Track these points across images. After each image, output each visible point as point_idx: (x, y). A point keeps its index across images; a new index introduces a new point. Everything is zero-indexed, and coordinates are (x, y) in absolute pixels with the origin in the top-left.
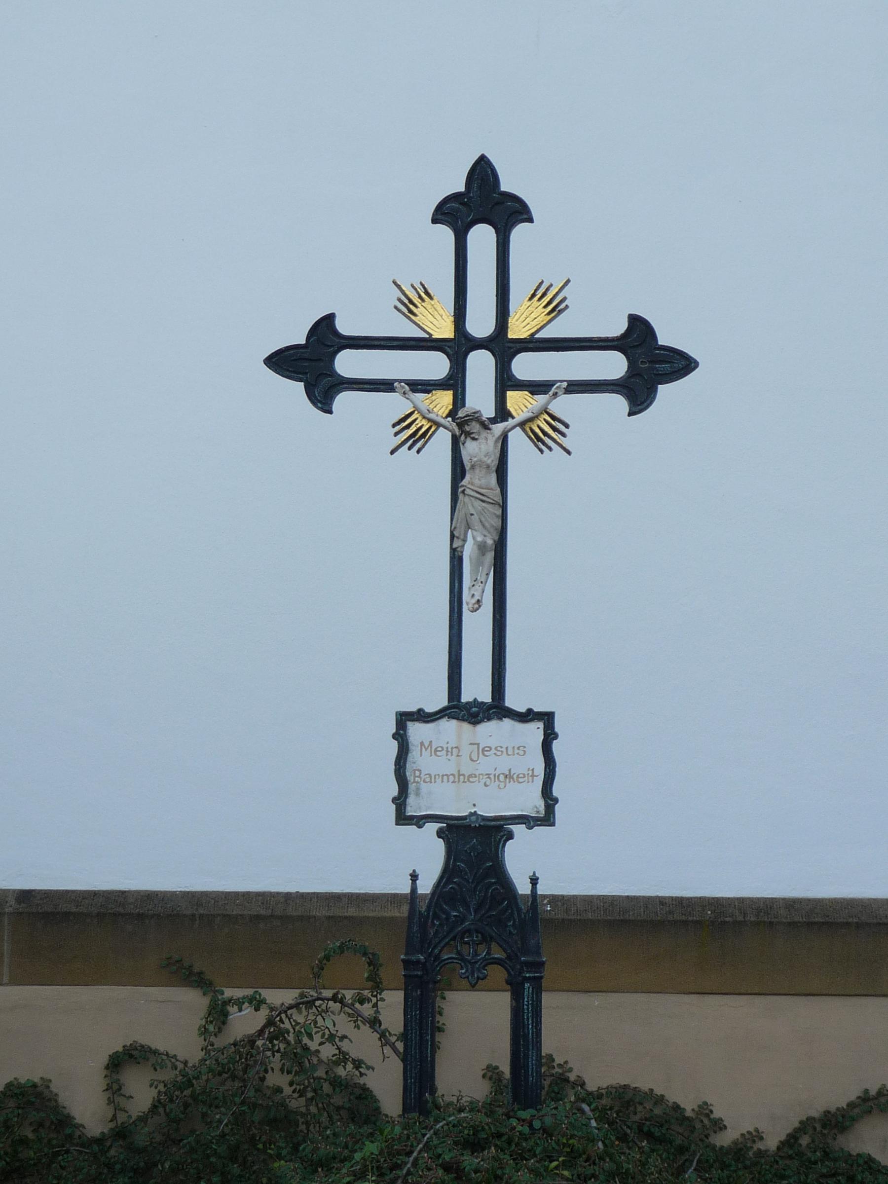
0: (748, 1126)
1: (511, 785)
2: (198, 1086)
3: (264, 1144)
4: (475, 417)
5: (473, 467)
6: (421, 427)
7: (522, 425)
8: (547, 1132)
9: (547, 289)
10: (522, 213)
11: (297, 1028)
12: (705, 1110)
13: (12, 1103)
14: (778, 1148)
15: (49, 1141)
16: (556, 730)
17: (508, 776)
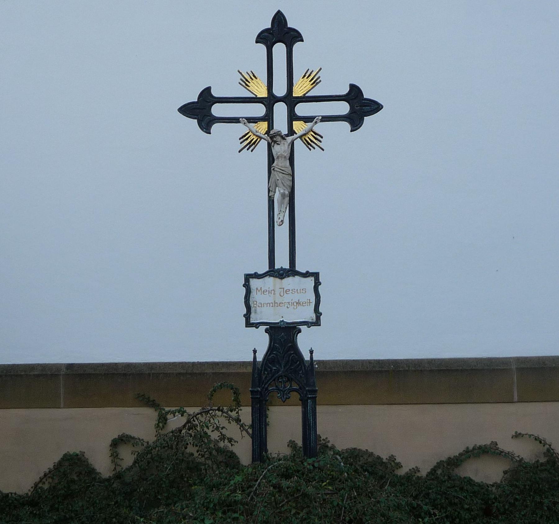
0: (412, 466)
1: (300, 308)
2: (154, 452)
3: (187, 478)
4: (279, 134)
5: (278, 158)
6: (253, 139)
7: (300, 137)
8: (320, 469)
9: (311, 73)
10: (298, 37)
11: (201, 424)
12: (392, 458)
13: (67, 464)
14: (427, 475)
15: (85, 480)
16: (320, 281)
17: (298, 303)
